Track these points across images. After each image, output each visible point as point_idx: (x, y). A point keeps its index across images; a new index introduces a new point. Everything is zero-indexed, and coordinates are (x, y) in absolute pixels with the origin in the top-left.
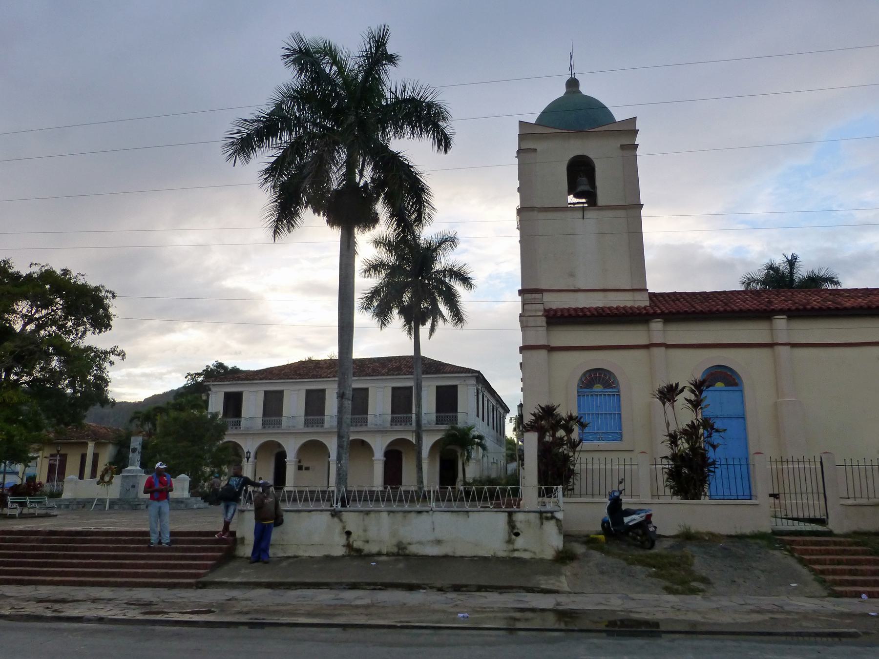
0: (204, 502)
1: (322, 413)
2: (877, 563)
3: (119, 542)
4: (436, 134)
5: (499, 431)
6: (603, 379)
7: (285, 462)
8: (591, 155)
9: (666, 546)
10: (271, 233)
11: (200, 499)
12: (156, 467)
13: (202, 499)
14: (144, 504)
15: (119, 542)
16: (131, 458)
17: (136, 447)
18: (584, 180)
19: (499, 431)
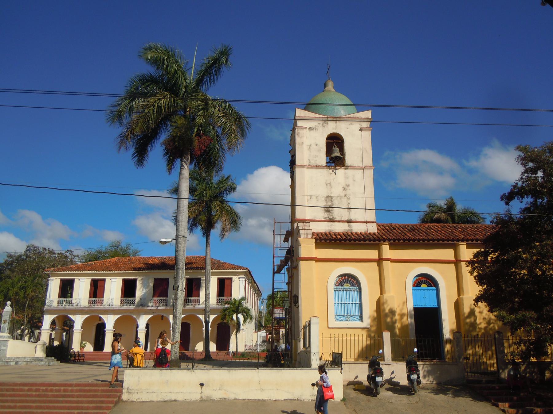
0: (57, 360)
1: (134, 296)
2: (1, 390)
3: (13, 390)
4: (180, 82)
5: (255, 310)
6: (350, 281)
7: (105, 331)
8: (342, 134)
9: (416, 384)
10: (168, 173)
11: (54, 358)
12: (536, 361)
13: (55, 358)
14: (13, 361)
15: (13, 390)
16: (3, 327)
17: (6, 319)
18: (337, 149)
19: (255, 310)
